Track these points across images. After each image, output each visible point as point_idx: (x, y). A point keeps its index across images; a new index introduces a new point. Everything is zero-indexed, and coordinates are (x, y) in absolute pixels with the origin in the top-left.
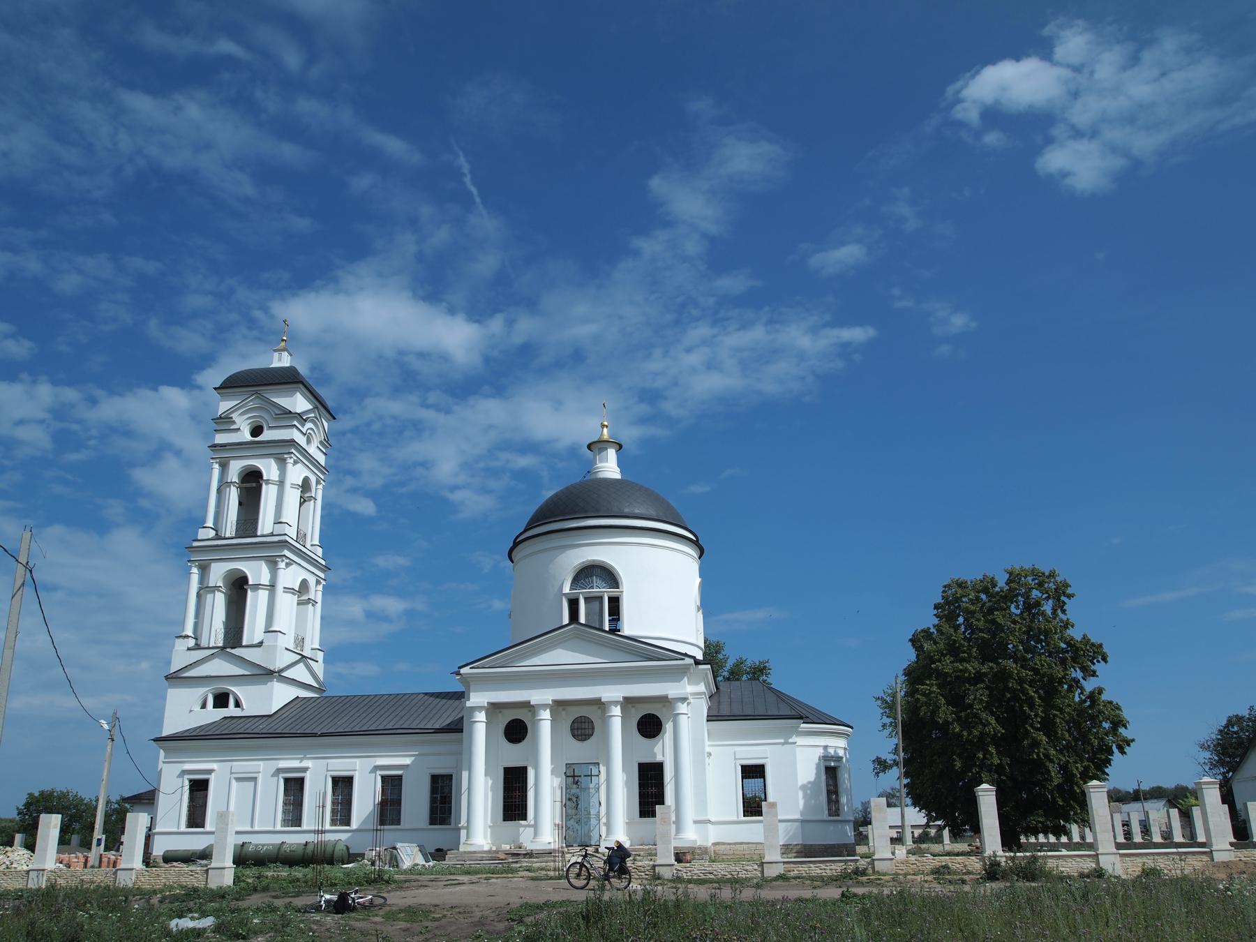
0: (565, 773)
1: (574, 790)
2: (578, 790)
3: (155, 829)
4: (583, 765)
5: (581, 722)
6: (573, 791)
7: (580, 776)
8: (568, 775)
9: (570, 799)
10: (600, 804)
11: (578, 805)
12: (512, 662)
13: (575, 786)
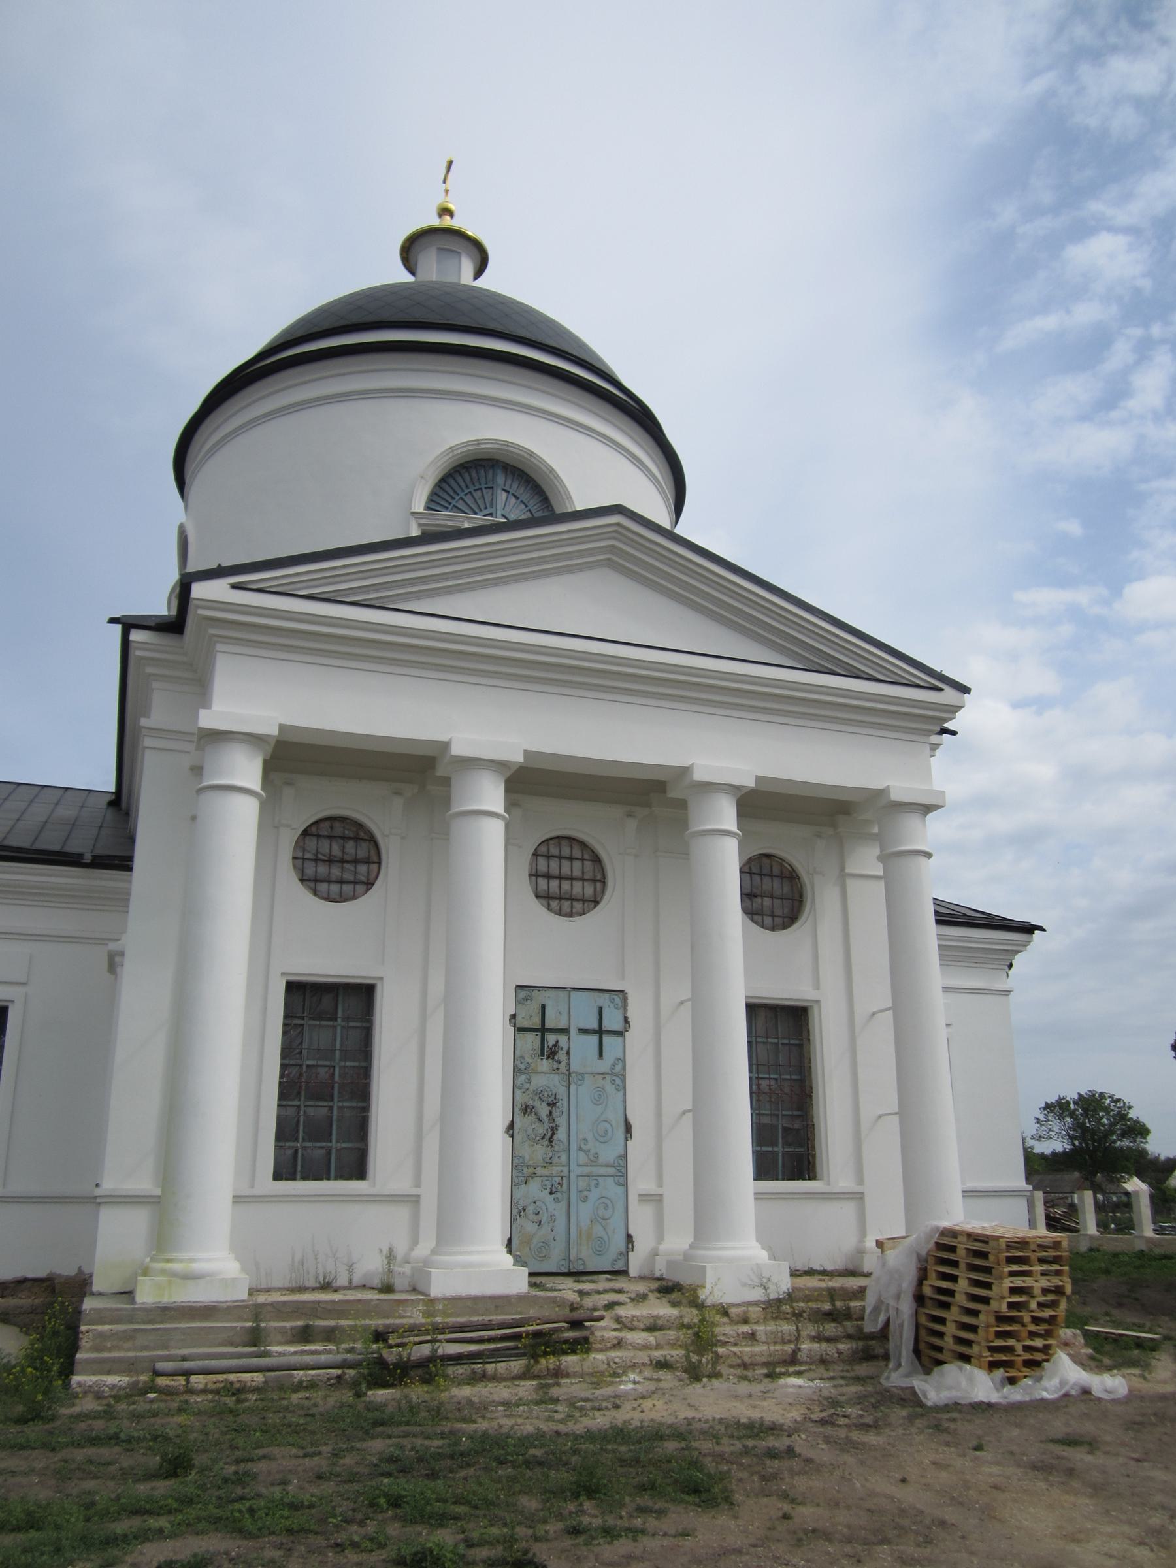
0: (513, 1016)
1: (545, 1078)
2: (556, 1078)
3: (147, 715)
4: (574, 994)
5: (761, 875)
6: (539, 1082)
7: (565, 1031)
8: (522, 1022)
9: (526, 1109)
10: (628, 1129)
11: (554, 1131)
12: (344, 595)
13: (545, 1065)
